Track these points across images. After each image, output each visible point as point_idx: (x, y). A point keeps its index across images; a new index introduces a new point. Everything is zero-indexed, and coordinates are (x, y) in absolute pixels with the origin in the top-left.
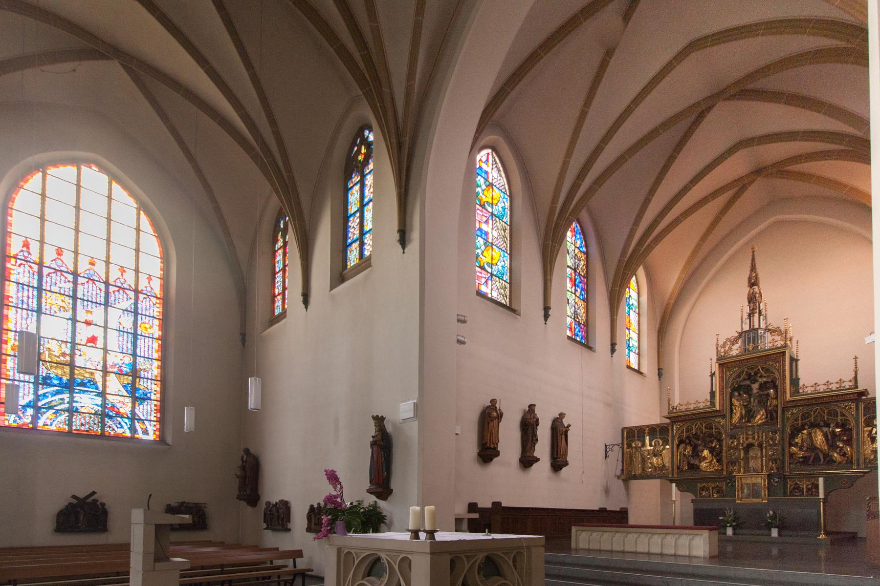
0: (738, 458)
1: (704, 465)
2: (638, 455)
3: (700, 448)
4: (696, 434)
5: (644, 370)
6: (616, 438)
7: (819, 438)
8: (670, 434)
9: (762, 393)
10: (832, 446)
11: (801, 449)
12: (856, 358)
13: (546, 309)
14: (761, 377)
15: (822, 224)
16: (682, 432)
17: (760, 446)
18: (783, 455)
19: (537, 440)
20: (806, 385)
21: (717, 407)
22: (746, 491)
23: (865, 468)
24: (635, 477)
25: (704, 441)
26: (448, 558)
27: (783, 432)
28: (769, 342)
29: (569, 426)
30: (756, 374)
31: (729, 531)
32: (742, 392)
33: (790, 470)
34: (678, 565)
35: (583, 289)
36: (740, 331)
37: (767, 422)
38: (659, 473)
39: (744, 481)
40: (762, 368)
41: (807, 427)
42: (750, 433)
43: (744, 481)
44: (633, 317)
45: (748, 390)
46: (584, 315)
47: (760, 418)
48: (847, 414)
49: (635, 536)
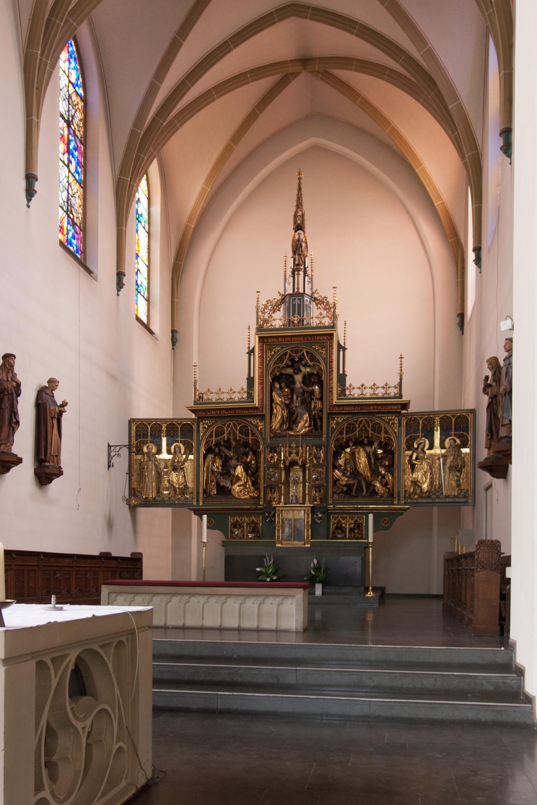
0: (279, 481)
1: (236, 488)
2: (151, 466)
3: (233, 462)
4: (229, 439)
5: (155, 327)
6: (120, 436)
7: (362, 460)
8: (195, 437)
9: (306, 388)
10: (375, 472)
11: (344, 474)
12: (401, 358)
13: (30, 179)
14: (305, 366)
15: (359, 166)
16: (211, 436)
17: (303, 467)
18: (327, 482)
19: (18, 423)
20: (354, 385)
21: (256, 403)
22: (287, 530)
23: (406, 503)
24: (148, 503)
25: (236, 452)
26: (32, 665)
27: (327, 447)
28: (315, 317)
29: (64, 404)
30: (301, 359)
31: (318, 590)
32: (283, 385)
33: (333, 503)
34: (284, 647)
35: (78, 163)
36: (282, 292)
37: (311, 431)
38: (177, 500)
39: (285, 515)
40: (308, 353)
41: (351, 444)
42: (293, 445)
43: (285, 515)
44: (142, 236)
45: (290, 381)
46: (80, 211)
47: (303, 426)
48: (390, 431)
49: (202, 599)
